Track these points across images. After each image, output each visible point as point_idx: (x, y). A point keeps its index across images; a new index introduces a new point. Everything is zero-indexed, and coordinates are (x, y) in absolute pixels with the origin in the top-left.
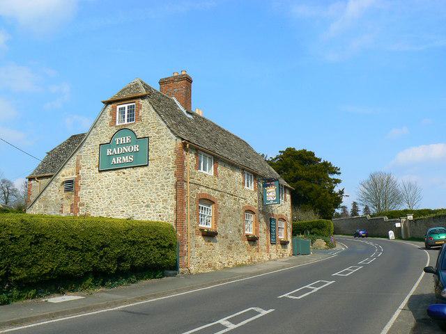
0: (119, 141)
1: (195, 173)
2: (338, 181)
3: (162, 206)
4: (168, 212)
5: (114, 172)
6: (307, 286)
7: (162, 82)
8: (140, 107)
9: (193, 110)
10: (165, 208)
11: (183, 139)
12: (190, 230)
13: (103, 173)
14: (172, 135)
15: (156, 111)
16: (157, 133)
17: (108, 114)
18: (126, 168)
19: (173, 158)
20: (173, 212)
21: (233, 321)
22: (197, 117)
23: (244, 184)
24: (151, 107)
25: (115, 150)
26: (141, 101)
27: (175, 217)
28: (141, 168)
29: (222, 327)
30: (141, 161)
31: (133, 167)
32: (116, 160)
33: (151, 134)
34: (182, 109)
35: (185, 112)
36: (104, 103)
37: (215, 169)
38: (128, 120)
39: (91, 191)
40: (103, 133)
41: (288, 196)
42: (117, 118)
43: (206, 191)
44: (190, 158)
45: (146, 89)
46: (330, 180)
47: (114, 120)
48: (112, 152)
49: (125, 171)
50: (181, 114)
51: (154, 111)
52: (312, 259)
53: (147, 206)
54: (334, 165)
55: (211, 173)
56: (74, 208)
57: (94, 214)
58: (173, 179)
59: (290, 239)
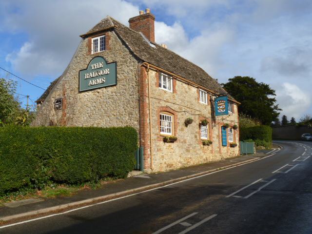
0: (94, 66)
1: (155, 90)
2: (274, 100)
5: (90, 93)
12: (153, 137)
13: (83, 94)
18: (100, 88)
23: (198, 99)
25: (91, 74)
29: (181, 228)
31: (105, 87)
33: (118, 59)
35: (149, 43)
36: (81, 36)
38: (100, 49)
41: (235, 108)
47: (90, 51)
48: (96, 82)
49: (99, 90)
52: (15, 79)
54: (271, 87)
56: (235, 128)
58: (136, 97)
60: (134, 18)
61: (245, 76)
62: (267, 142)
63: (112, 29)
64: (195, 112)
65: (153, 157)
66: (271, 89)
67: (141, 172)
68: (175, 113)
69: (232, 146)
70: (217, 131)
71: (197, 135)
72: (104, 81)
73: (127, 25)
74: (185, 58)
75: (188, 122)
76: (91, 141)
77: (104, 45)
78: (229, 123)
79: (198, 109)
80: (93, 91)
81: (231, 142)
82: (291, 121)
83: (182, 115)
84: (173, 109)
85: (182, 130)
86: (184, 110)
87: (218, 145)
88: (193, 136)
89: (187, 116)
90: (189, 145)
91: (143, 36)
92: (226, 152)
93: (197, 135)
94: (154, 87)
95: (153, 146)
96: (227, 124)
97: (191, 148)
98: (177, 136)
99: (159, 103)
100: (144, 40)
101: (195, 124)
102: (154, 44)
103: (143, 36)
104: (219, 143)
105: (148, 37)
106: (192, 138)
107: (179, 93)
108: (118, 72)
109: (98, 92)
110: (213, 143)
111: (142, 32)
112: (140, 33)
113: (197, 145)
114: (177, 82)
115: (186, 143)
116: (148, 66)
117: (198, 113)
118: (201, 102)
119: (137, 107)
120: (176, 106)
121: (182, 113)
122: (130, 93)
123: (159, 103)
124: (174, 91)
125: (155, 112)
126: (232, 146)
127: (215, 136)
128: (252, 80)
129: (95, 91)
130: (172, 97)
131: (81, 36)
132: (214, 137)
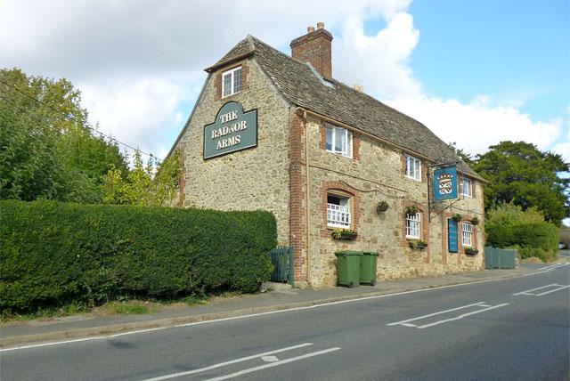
3: (273, 198)
4: (281, 207)
6: (401, 323)
7: (294, 44)
8: (246, 69)
9: (334, 76)
10: (277, 201)
11: (298, 106)
12: (313, 230)
13: (209, 162)
14: (285, 102)
15: (265, 72)
16: (268, 102)
17: (213, 85)
19: (285, 134)
20: (286, 206)
21: (280, 356)
22: (340, 88)
23: (405, 171)
24: (260, 69)
26: (248, 62)
27: (288, 213)
28: (250, 152)
30: (251, 142)
31: (240, 151)
32: (222, 142)
34: (318, 76)
35: (321, 79)
37: (356, 149)
39: (197, 186)
40: (208, 110)
42: (223, 90)
43: (334, 177)
44: (313, 129)
45: (256, 46)
46: (560, 181)
49: (231, 156)
50: (315, 81)
51: (262, 73)
53: (257, 200)
55: (347, 152)
57: (199, 205)
58: (286, 162)
59: (481, 249)
60: (298, 39)
61: (518, 141)
62: (546, 250)
63: (250, 56)
64: (396, 193)
65: (311, 263)
66: (565, 162)
67: (288, 286)
68: (355, 192)
69: (470, 253)
70: (437, 229)
71: (400, 231)
72: (239, 140)
73: (289, 53)
74: (407, 114)
75: (382, 208)
76: (190, 230)
77: (241, 78)
78: (461, 213)
79: (401, 188)
80: (223, 158)
81: (469, 246)
82: (164, 165)
83: (371, 196)
84: (353, 185)
85: (370, 221)
86: (373, 189)
87: (440, 250)
88: (391, 231)
89: (378, 199)
90: (382, 247)
91: (313, 69)
92: (456, 261)
93: (400, 231)
94: (318, 150)
95: (313, 245)
96: (458, 215)
97: (386, 252)
98: (359, 231)
99: (326, 175)
100: (312, 75)
101: (395, 214)
102: (332, 82)
103: (313, 69)
104: (443, 245)
105: (321, 71)
106: (389, 236)
107: (362, 158)
108: (260, 124)
109: (231, 160)
110: (430, 246)
111: (310, 61)
112: (307, 63)
113: (398, 248)
114: (362, 143)
115: (376, 242)
116: (305, 114)
117: (403, 194)
118: (408, 176)
119: (285, 182)
120: (358, 181)
121: (371, 193)
122: (277, 158)
123: (326, 175)
124: (356, 156)
125: (318, 190)
126: (470, 253)
127: (435, 235)
128: (530, 146)
129: (226, 157)
130: (350, 167)
131: (207, 71)
132: (432, 237)
